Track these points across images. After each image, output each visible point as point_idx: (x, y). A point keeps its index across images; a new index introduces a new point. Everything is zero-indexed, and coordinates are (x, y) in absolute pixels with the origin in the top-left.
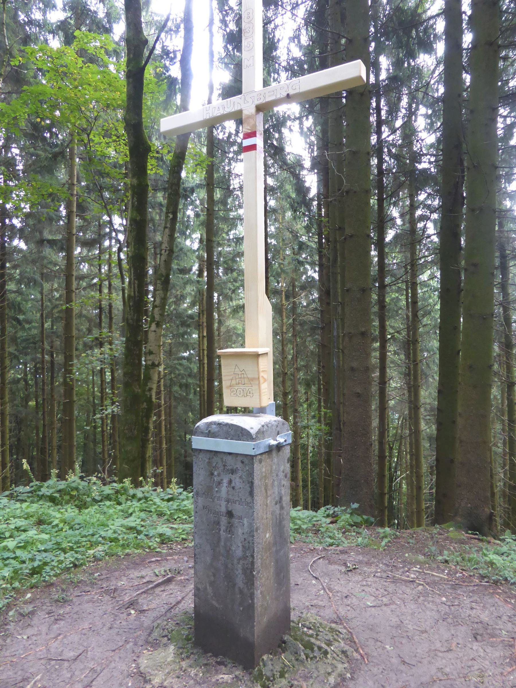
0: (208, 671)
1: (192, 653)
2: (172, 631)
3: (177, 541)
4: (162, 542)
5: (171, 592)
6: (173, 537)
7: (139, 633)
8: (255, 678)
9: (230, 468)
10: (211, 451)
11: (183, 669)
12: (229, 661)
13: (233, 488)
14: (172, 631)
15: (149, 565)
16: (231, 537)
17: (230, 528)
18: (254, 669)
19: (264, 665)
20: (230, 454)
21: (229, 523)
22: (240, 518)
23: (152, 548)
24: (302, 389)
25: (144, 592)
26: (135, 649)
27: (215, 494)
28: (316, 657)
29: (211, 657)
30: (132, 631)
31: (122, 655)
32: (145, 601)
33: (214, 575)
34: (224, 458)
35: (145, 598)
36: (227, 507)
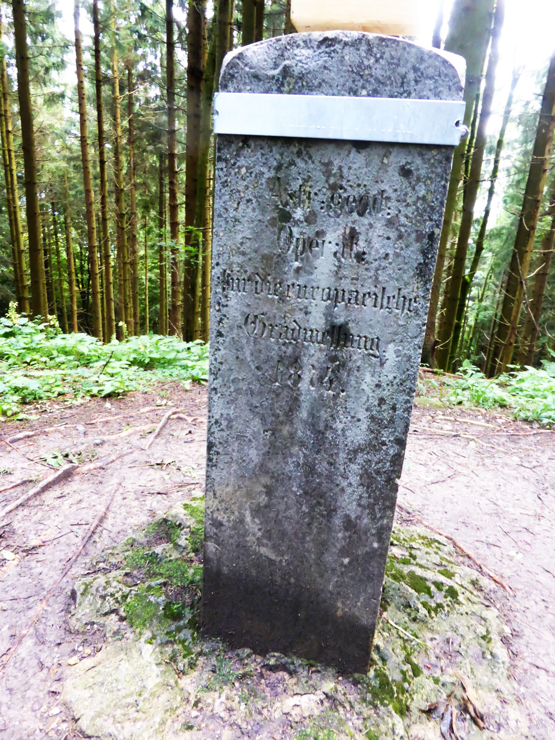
0: (253, 693)
1: (200, 654)
2: (125, 597)
3: (49, 398)
4: (24, 402)
5: (77, 497)
6: (41, 391)
7: (39, 608)
8: (375, 695)
9: (354, 193)
10: (287, 141)
11: (193, 700)
12: (298, 662)
13: (360, 257)
14: (125, 597)
15: (15, 445)
16: (335, 397)
17: (335, 373)
18: (366, 672)
19: (384, 660)
20: (360, 145)
21: (333, 359)
22: (376, 343)
23: (9, 413)
24: (139, 213)
25: (22, 505)
26: (43, 657)
27: (290, 279)
28: (439, 606)
29: (249, 656)
30: (19, 606)
31: (13, 683)
32: (27, 524)
33: (269, 491)
34: (337, 162)
35: (25, 518)
36: (329, 314)
